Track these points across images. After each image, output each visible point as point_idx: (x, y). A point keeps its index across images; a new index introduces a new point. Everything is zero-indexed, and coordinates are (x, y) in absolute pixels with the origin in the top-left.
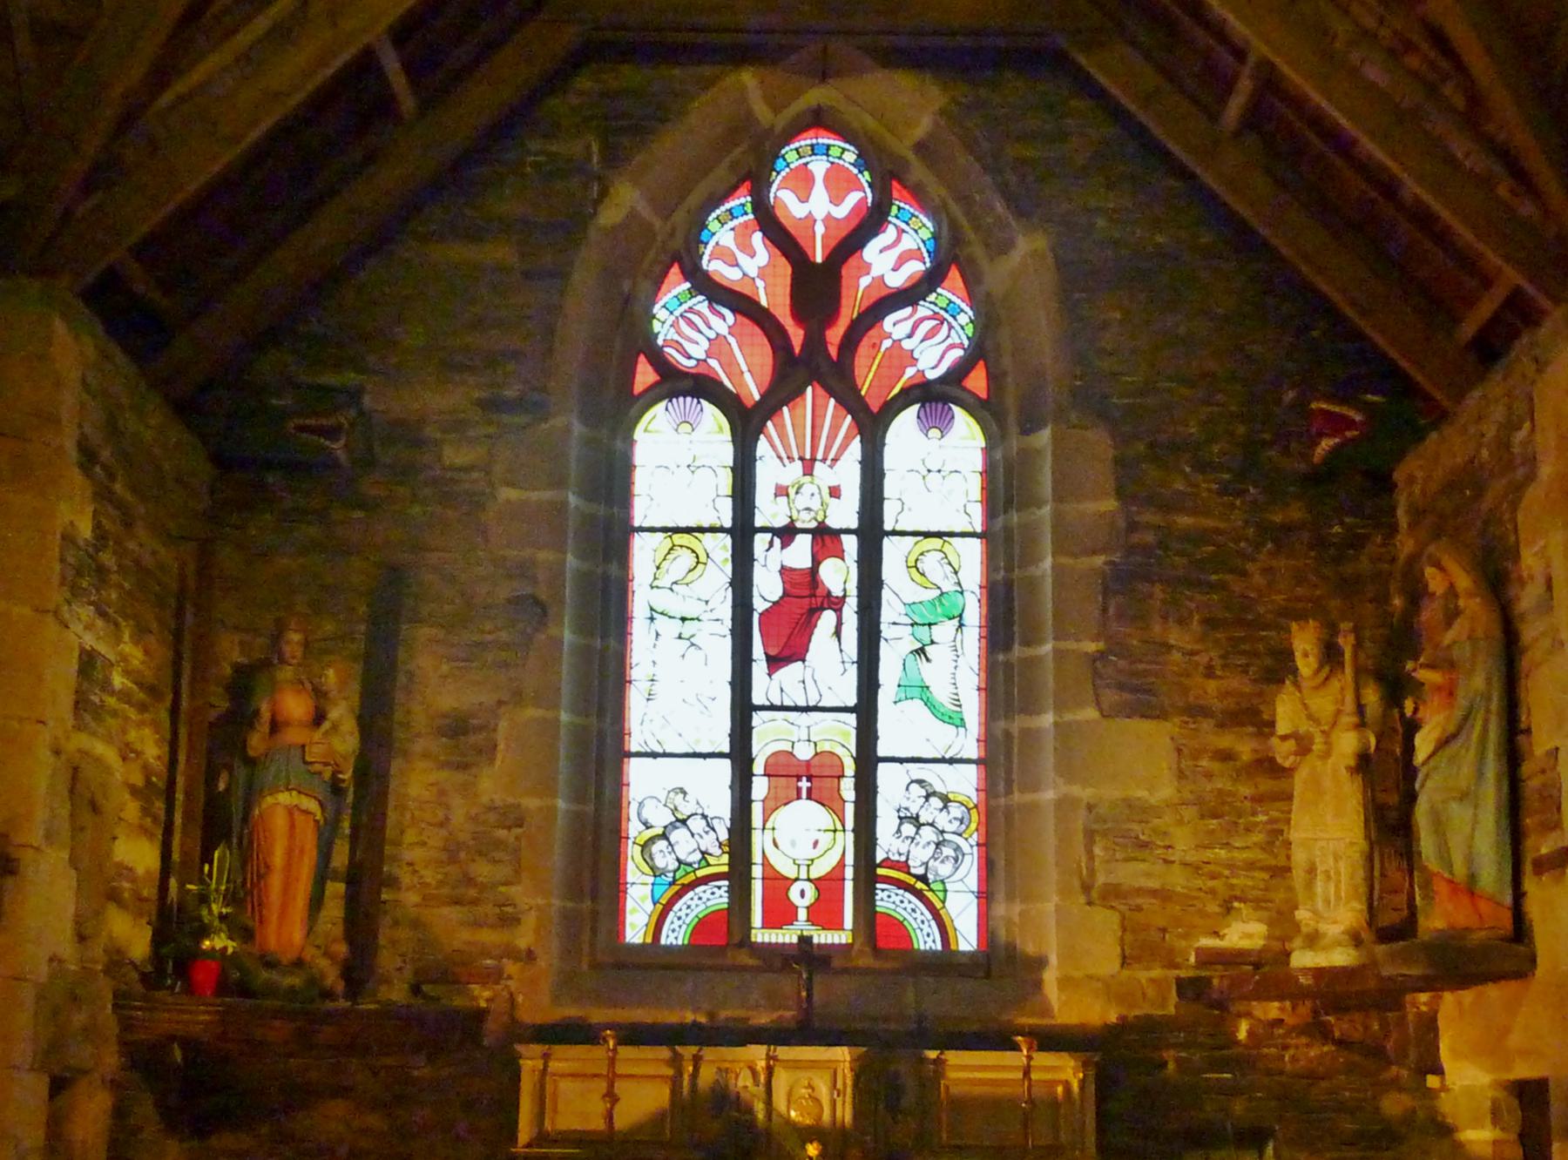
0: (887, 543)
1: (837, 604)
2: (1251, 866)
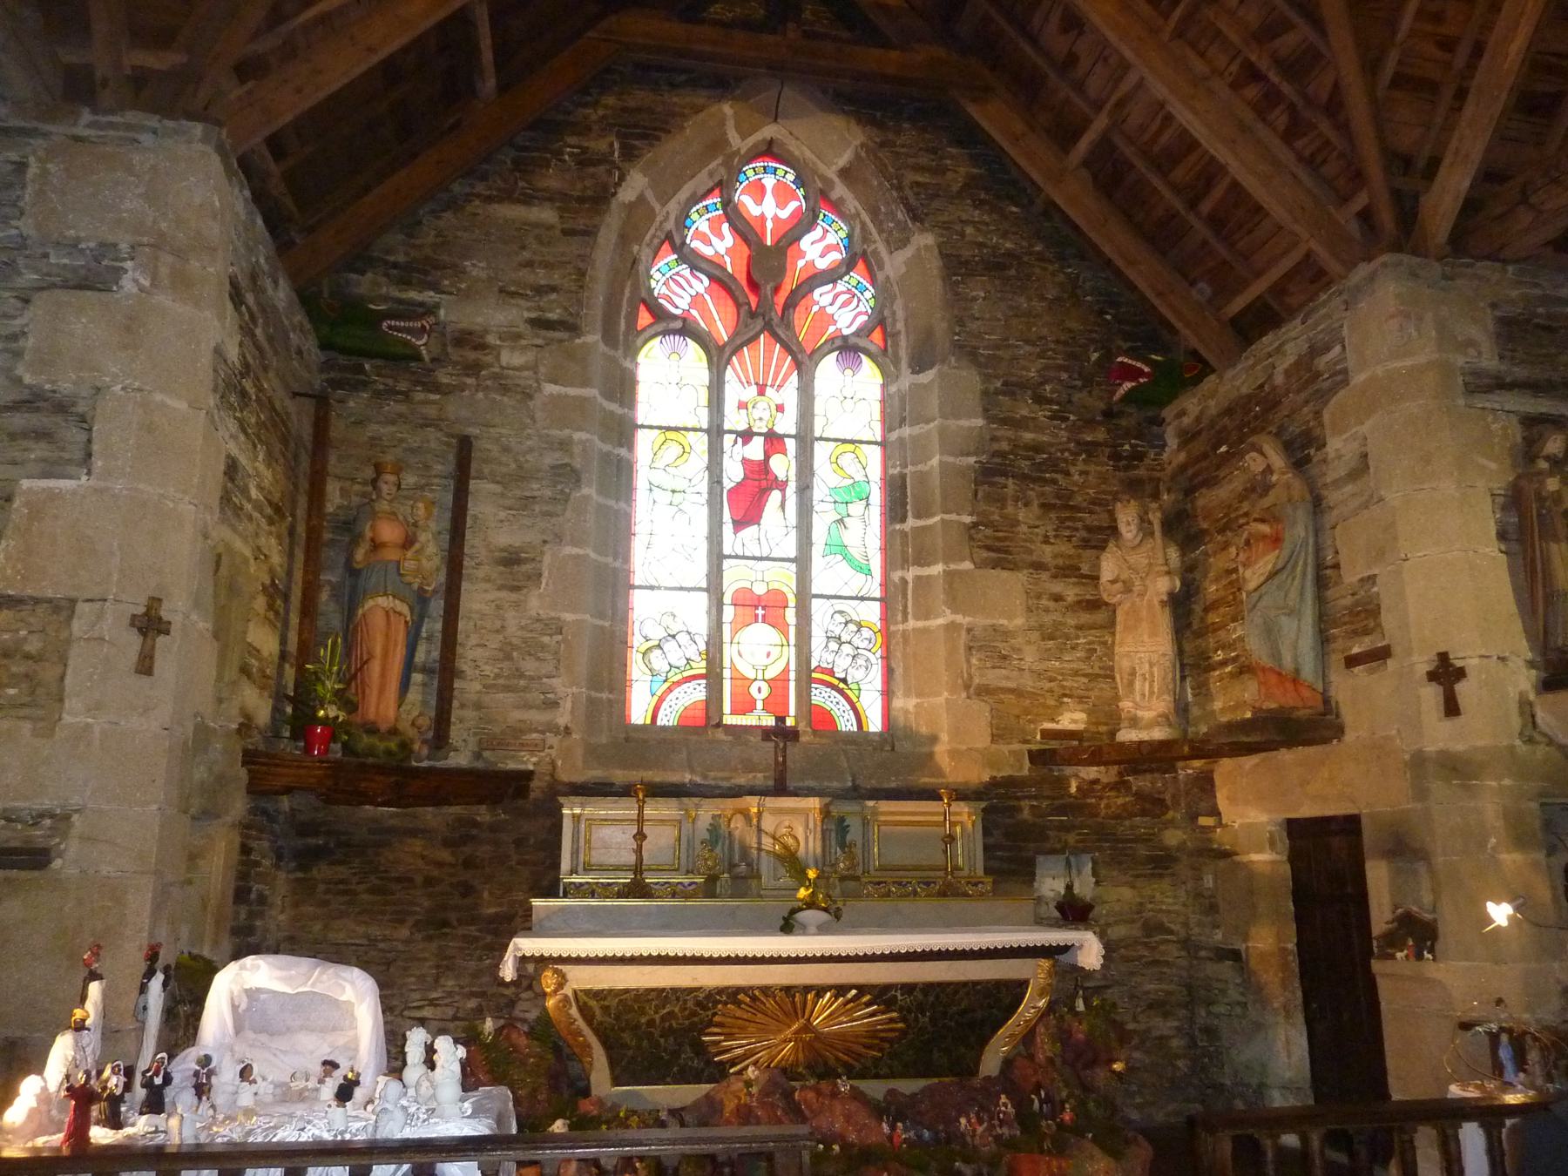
0: (817, 445)
1: (782, 486)
2: (1076, 673)
